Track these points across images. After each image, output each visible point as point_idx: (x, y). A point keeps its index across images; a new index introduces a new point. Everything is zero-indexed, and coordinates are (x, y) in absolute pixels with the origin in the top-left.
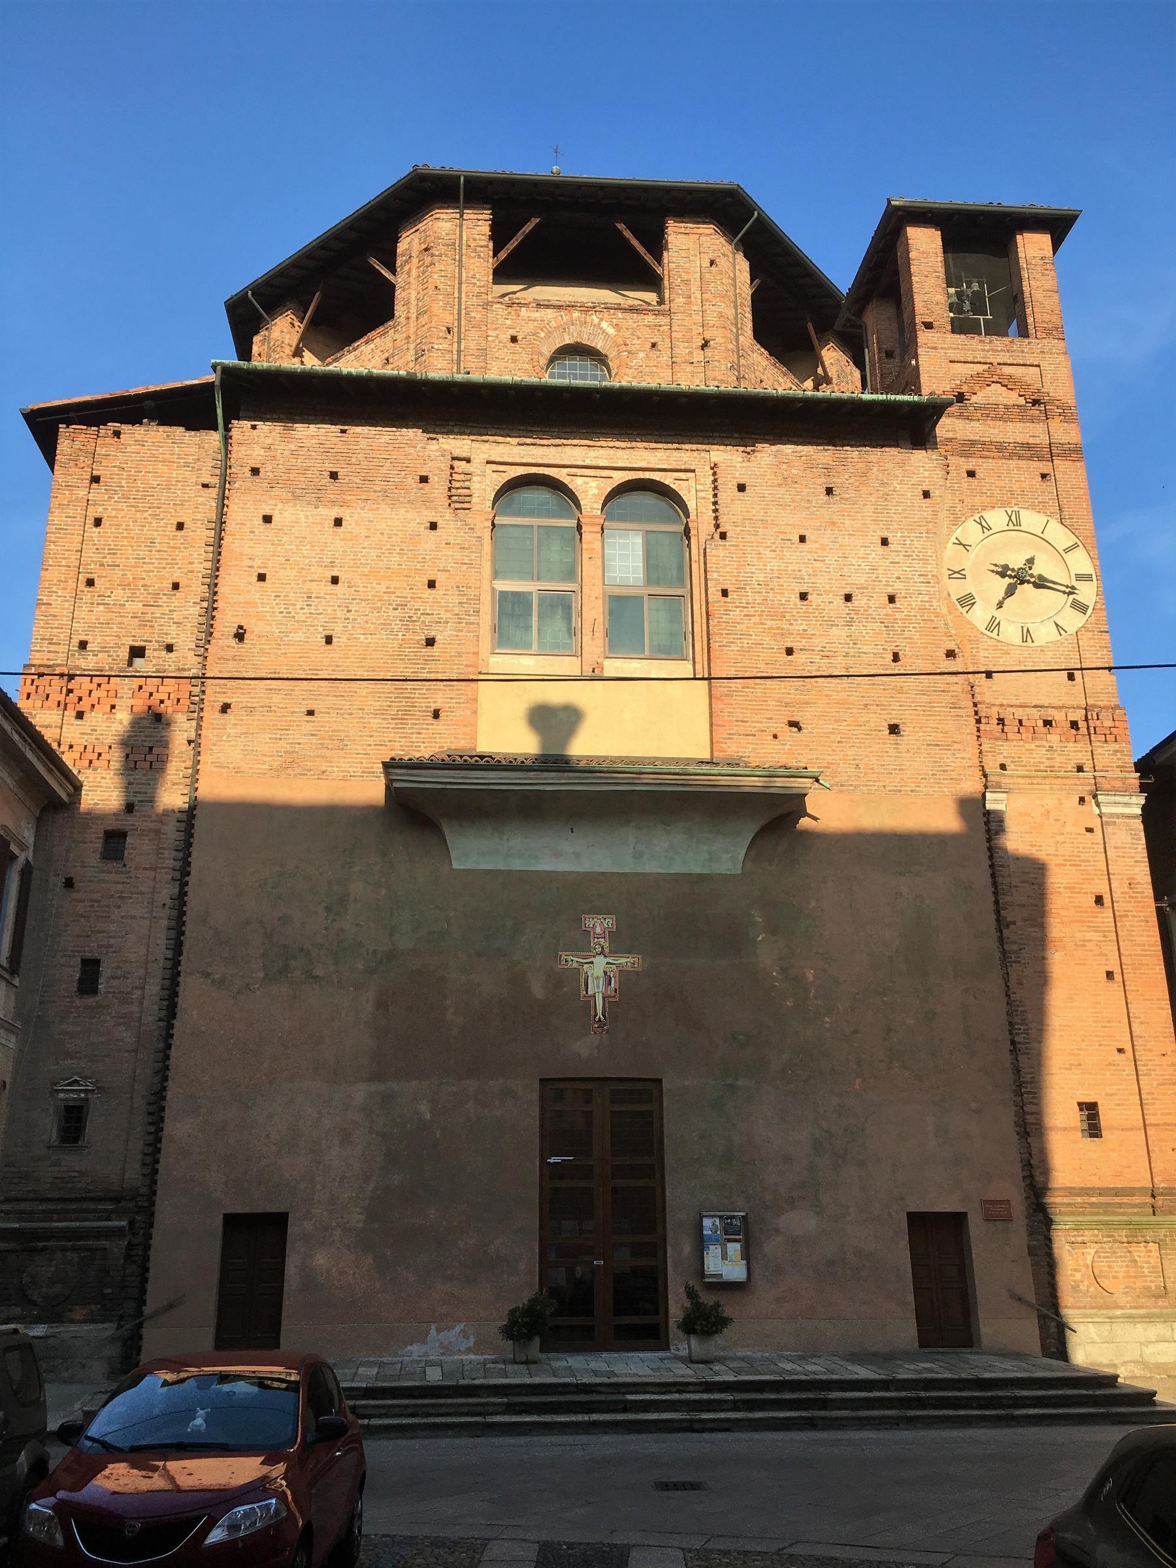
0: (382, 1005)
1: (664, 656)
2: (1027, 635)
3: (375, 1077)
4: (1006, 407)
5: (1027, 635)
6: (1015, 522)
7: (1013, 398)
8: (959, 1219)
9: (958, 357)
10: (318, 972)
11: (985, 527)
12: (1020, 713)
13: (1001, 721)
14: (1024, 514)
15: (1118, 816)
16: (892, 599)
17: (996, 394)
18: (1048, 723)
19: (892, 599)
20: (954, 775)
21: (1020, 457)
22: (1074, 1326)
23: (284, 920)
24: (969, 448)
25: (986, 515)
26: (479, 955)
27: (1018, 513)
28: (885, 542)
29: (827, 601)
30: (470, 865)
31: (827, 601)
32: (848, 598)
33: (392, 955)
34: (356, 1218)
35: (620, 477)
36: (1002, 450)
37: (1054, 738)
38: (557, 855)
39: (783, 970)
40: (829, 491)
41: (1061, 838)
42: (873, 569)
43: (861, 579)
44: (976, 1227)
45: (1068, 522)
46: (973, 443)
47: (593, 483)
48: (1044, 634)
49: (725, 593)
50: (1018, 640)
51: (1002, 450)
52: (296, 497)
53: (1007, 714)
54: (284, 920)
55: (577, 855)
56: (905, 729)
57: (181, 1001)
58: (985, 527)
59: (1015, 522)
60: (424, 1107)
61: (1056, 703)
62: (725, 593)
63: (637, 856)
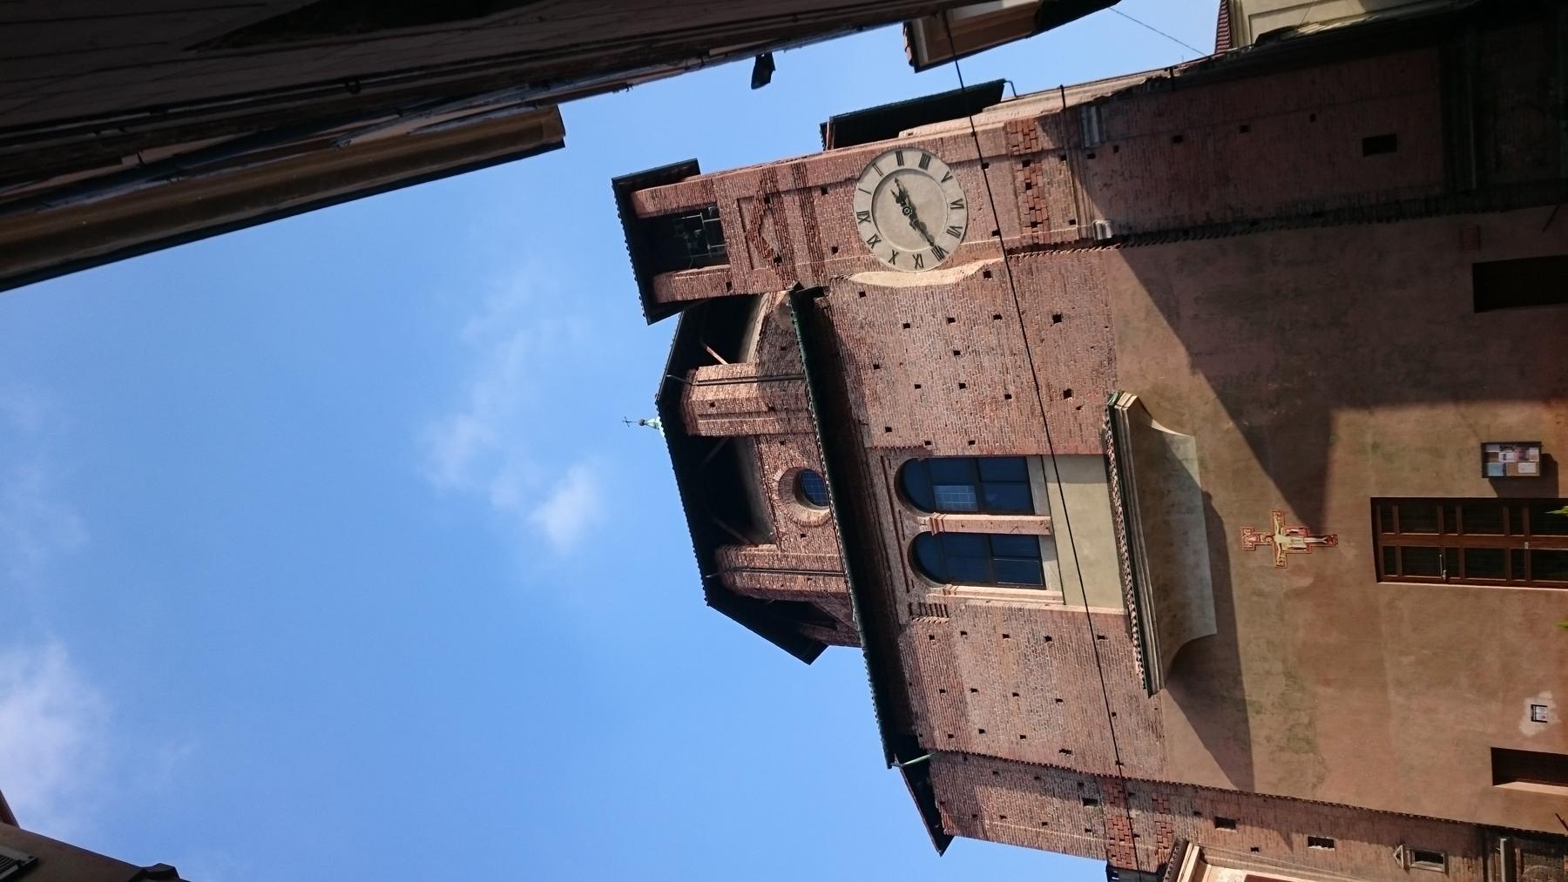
0: (1327, 683)
1: (1381, 561)
2: (957, 205)
3: (1384, 687)
4: (776, 223)
5: (957, 205)
6: (865, 216)
7: (769, 222)
8: (1480, 271)
9: (747, 263)
10: (1306, 721)
11: (875, 240)
12: (1024, 210)
13: (1034, 225)
14: (858, 209)
15: (1100, 128)
16: (951, 320)
17: (769, 232)
18: (1029, 186)
19: (951, 320)
20: (1087, 272)
21: (813, 211)
22: (920, 441)
23: (1269, 739)
24: (816, 253)
25: (866, 239)
26: (1282, 619)
27: (859, 214)
28: (907, 326)
29: (964, 368)
30: (1213, 623)
31: (964, 368)
32: (957, 353)
33: (1288, 675)
34: (1495, 707)
35: (898, 507)
36: (811, 228)
37: (1041, 181)
38: (1197, 566)
39: (1271, 406)
40: (876, 367)
41: (1127, 175)
42: (929, 335)
43: (940, 345)
44: (1487, 255)
45: (857, 175)
46: (811, 249)
47: (906, 522)
48: (953, 190)
49: (971, 443)
50: (963, 212)
51: (811, 228)
52: (963, 714)
53: (1026, 219)
54: (1269, 739)
55: (1195, 552)
56: (1057, 311)
57: (1335, 801)
58: (875, 240)
59: (865, 216)
60: (1406, 660)
61: (1010, 178)
62: (971, 443)
63: (1190, 511)
